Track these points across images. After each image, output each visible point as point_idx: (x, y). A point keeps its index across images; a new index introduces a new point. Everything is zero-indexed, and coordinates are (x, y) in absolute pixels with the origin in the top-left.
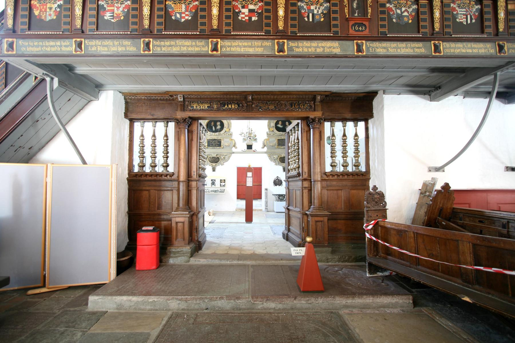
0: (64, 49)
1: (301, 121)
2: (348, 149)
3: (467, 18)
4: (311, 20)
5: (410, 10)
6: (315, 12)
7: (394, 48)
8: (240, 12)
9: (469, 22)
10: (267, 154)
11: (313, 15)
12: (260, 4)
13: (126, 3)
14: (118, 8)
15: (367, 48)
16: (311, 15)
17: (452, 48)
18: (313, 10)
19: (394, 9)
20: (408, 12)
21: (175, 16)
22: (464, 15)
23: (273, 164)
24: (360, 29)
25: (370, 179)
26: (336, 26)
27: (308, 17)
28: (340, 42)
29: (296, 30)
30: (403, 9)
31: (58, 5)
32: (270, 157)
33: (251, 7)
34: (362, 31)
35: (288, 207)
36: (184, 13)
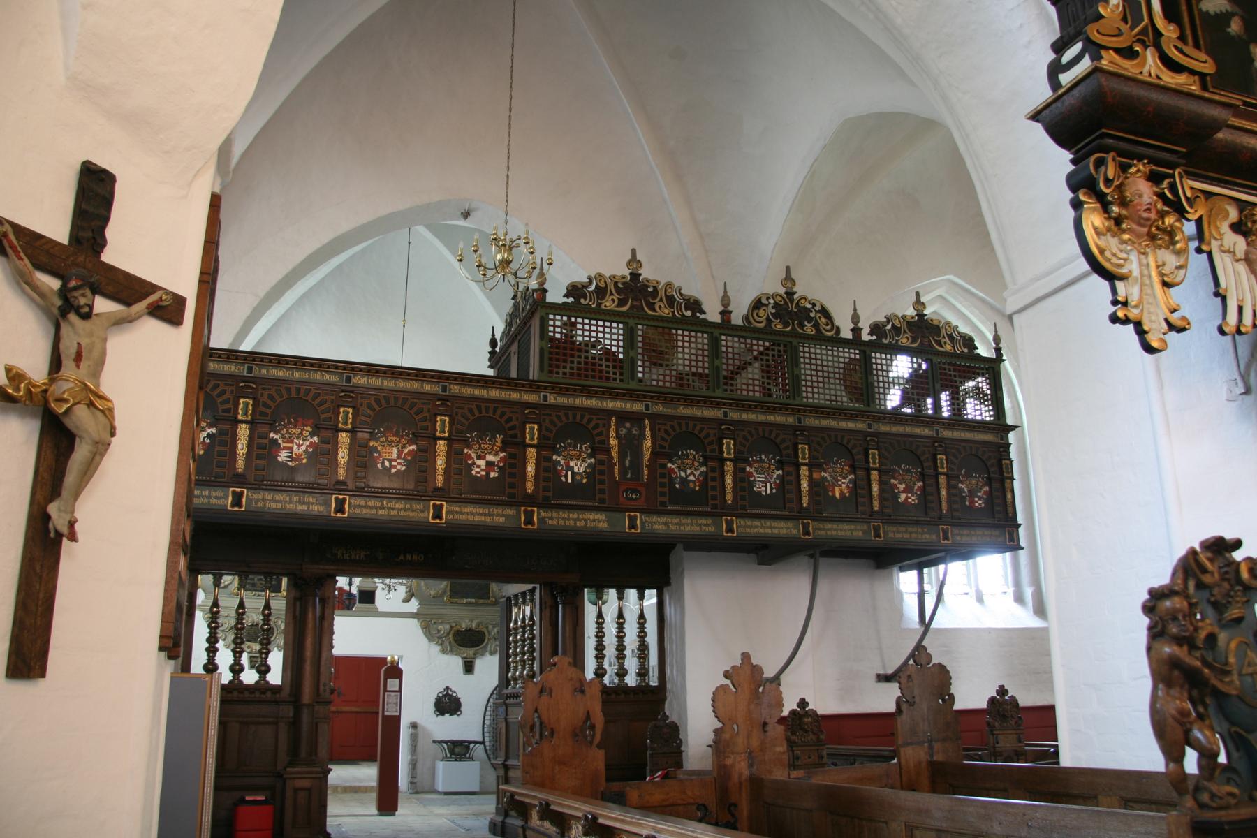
0: (213, 501)
1: (540, 586)
2: (627, 641)
3: (766, 487)
4: (569, 481)
5: (697, 473)
6: (576, 470)
7: (676, 524)
8: (475, 464)
9: (769, 492)
10: (419, 619)
11: (573, 473)
12: (502, 455)
13: (311, 440)
14: (299, 446)
15: (642, 523)
16: (569, 473)
17: (747, 527)
18: (573, 467)
19: (677, 470)
20: (694, 475)
21: (383, 463)
22: (762, 482)
23: (435, 649)
24: (634, 496)
25: (665, 699)
26: (602, 492)
27: (566, 476)
28: (608, 513)
29: (550, 494)
30: (689, 471)
31: (208, 434)
32: (428, 629)
33: (490, 458)
34: (636, 499)
35: (506, 760)
36: (395, 460)
